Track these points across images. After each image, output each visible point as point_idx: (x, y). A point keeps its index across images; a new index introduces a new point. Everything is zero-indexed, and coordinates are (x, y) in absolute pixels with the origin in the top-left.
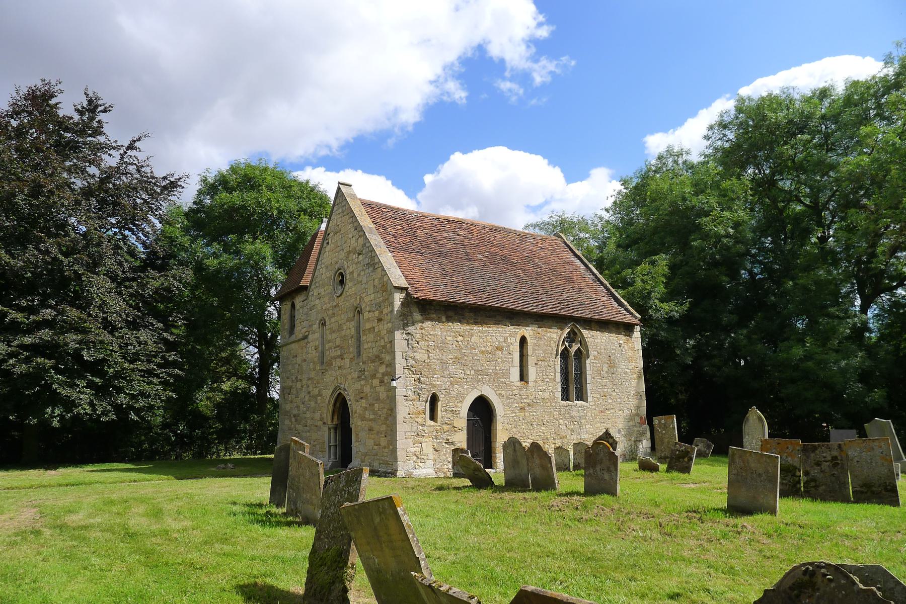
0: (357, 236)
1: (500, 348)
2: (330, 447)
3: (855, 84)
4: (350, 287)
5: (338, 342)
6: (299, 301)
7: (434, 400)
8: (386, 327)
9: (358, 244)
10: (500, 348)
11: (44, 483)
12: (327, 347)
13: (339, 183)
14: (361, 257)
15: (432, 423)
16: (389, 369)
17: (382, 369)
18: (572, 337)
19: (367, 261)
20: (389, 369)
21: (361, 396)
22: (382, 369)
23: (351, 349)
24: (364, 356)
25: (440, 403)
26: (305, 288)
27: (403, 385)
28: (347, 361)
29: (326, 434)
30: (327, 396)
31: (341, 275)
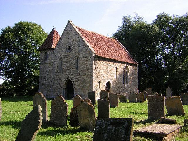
0: (77, 37)
1: (112, 70)
2: (64, 93)
3: (165, 15)
4: (73, 51)
5: (68, 65)
6: (49, 52)
7: (100, 82)
8: (89, 63)
9: (79, 39)
10: (112, 70)
11: (138, 111)
12: (63, 66)
13: (69, 20)
14: (78, 43)
15: (99, 88)
16: (90, 74)
17: (87, 74)
18: (126, 67)
19: (81, 44)
20: (90, 74)
21: (77, 80)
22: (87, 74)
23: (74, 68)
24: (80, 70)
25: (101, 83)
26: (53, 49)
27: (94, 79)
28: (72, 71)
29: (63, 90)
30: (63, 80)
31: (70, 47)
